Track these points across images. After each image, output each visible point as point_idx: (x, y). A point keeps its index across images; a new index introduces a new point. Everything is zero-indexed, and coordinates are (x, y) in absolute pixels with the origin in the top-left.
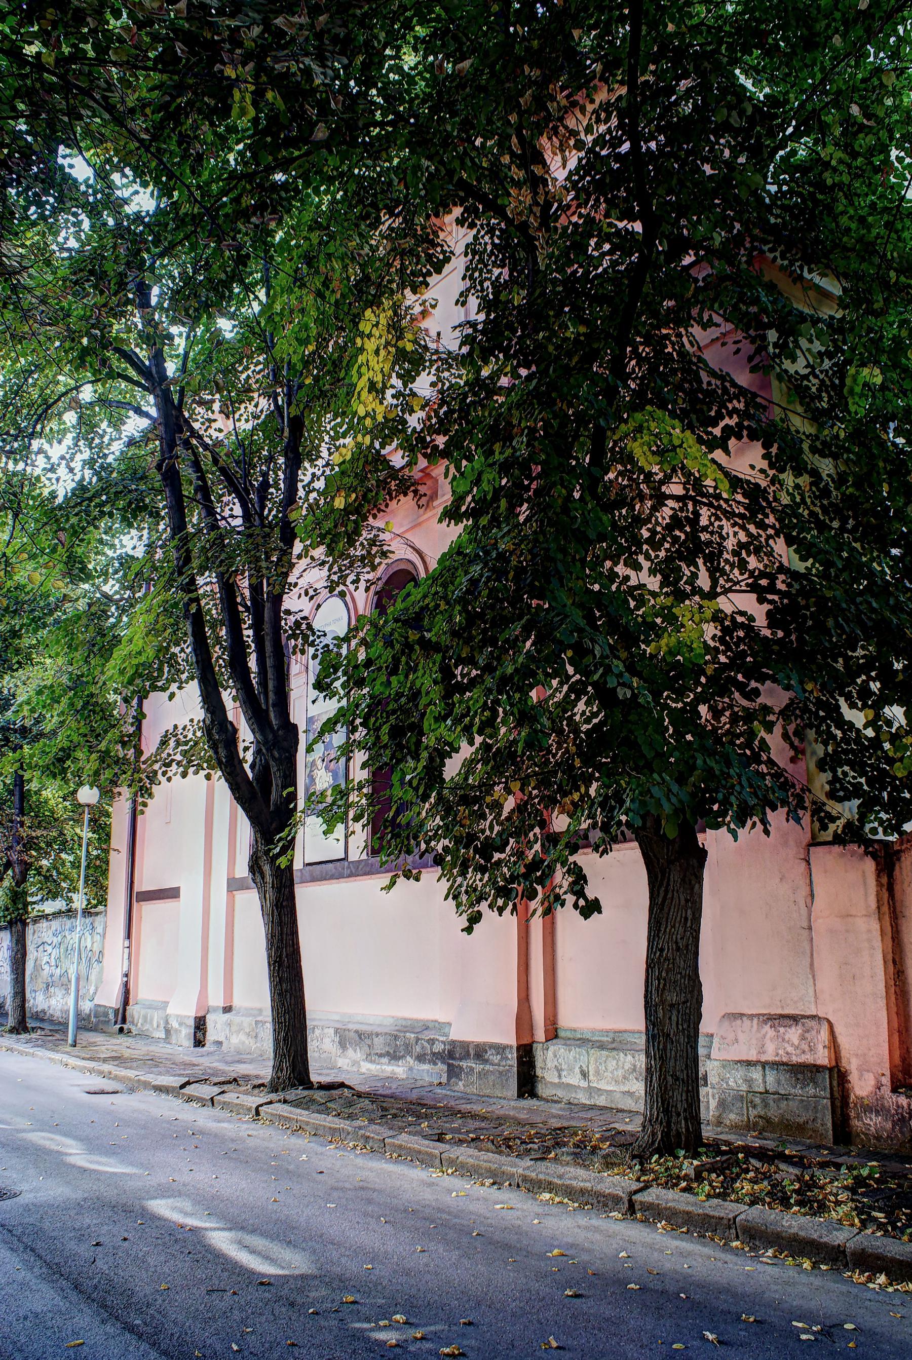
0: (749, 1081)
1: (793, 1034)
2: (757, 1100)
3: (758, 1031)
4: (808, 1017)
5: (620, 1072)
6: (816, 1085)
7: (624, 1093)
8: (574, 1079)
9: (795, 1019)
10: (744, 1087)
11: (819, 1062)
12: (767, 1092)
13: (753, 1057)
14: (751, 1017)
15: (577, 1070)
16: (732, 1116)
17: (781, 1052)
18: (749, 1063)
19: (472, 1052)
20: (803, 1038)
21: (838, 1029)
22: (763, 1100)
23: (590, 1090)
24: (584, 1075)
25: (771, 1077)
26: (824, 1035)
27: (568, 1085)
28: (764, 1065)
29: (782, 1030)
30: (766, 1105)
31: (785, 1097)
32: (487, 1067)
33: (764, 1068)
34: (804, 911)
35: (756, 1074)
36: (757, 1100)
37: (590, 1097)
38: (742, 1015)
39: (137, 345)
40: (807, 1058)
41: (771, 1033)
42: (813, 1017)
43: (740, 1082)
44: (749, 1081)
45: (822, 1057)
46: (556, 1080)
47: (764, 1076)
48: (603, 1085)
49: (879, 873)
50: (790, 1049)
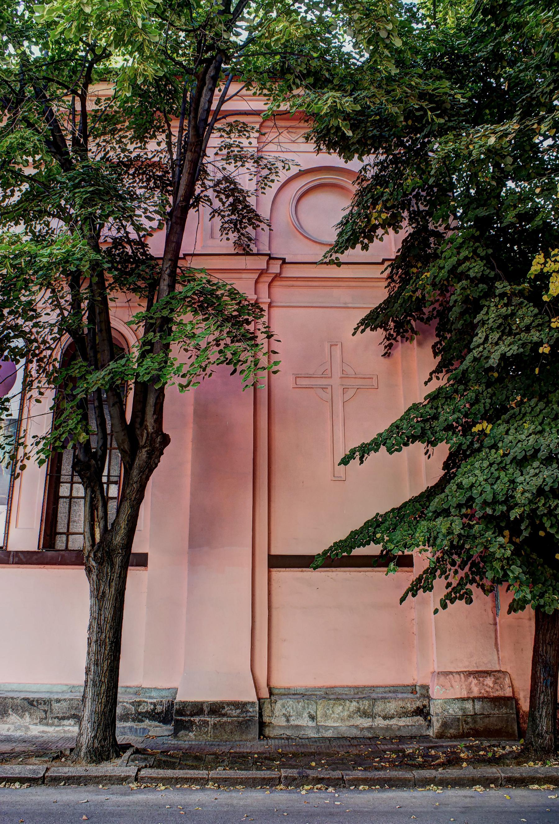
0: (463, 709)
1: (489, 681)
2: (469, 720)
3: (466, 680)
4: (496, 671)
5: (346, 713)
6: (507, 706)
7: (350, 726)
8: (305, 721)
9: (488, 673)
10: (460, 713)
11: (507, 695)
12: (476, 714)
13: (464, 694)
14: (458, 673)
15: (306, 715)
16: (452, 731)
17: (483, 691)
18: (463, 699)
19: (206, 710)
20: (495, 683)
21: (513, 677)
22: (473, 719)
23: (318, 728)
24: (312, 718)
25: (478, 706)
26: (507, 681)
27: (297, 726)
28: (473, 699)
29: (481, 679)
30: (475, 722)
31: (488, 716)
32: (225, 719)
33: (473, 701)
34: (491, 615)
35: (469, 705)
36: (469, 720)
37: (318, 732)
38: (451, 673)
39: (59, 174)
40: (500, 693)
41: (475, 681)
42: (499, 671)
43: (457, 710)
44: (463, 709)
45: (508, 692)
46: (285, 724)
47: (474, 706)
48: (330, 723)
49: (99, 596)
50: (488, 689)
